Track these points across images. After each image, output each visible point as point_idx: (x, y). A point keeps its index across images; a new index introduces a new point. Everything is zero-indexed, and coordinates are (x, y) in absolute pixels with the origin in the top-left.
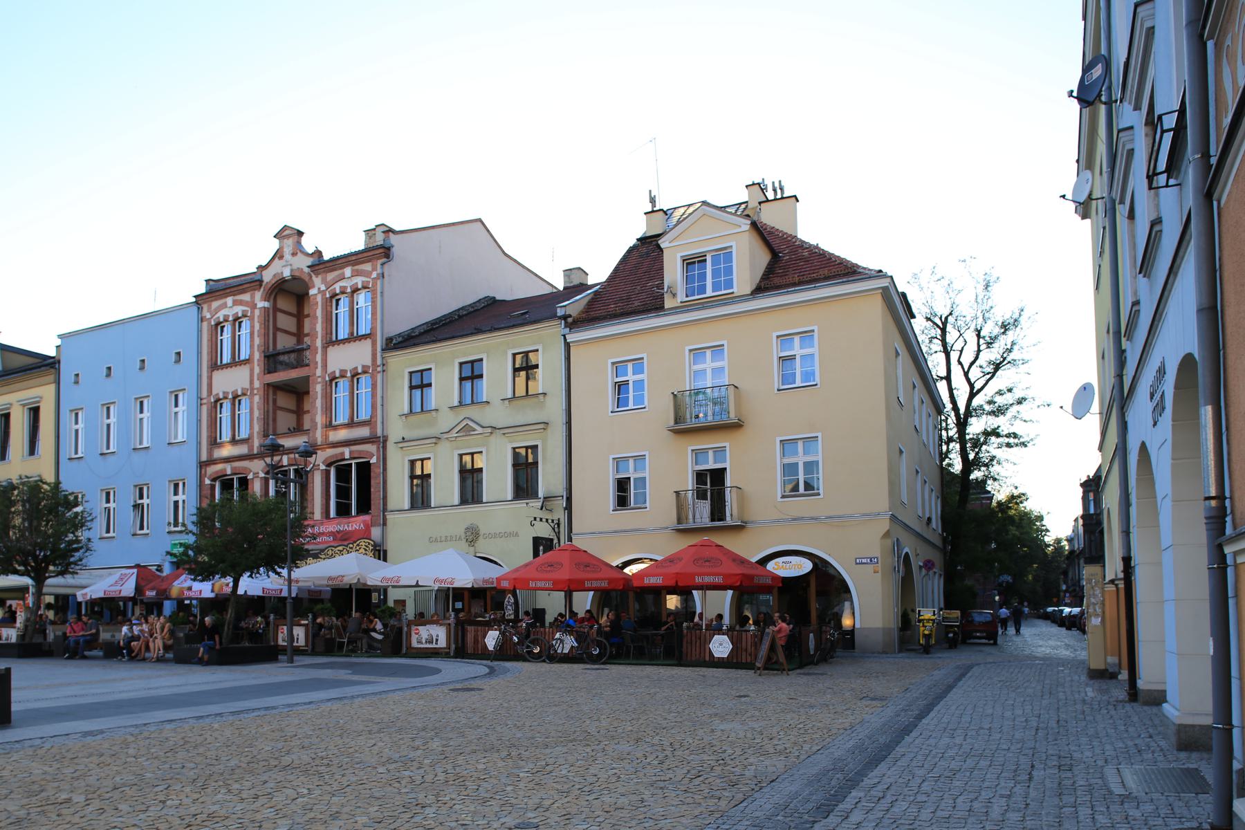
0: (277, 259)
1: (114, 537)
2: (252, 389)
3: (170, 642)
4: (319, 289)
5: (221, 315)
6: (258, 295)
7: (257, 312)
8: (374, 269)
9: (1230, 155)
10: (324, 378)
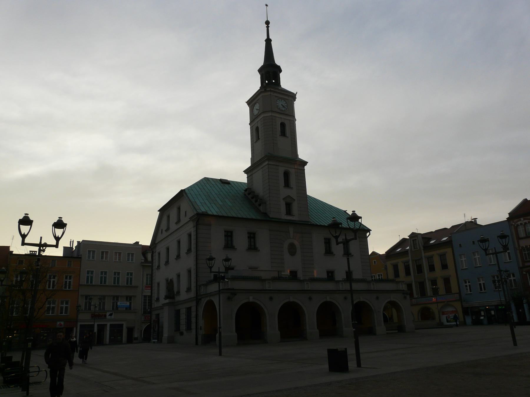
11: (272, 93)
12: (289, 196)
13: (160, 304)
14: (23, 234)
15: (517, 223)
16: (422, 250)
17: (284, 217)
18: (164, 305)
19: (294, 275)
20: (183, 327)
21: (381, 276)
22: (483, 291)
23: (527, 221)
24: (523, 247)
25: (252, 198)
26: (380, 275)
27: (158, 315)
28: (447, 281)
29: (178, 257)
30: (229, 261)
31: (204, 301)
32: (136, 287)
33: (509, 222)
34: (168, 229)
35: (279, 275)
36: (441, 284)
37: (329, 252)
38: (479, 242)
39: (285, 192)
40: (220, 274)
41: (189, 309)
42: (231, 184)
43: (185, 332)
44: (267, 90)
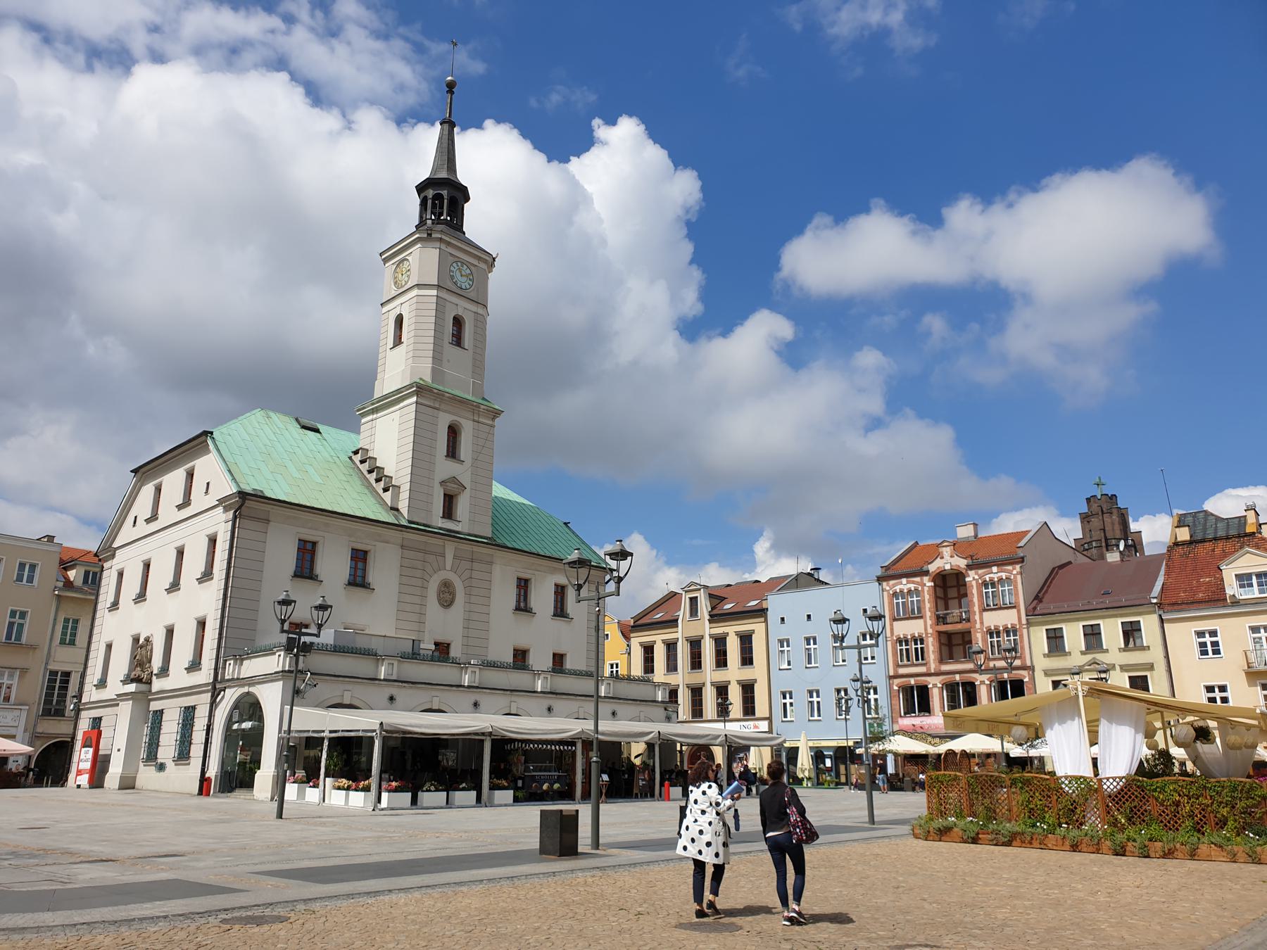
0: (939, 558)
1: (792, 721)
2: (927, 634)
3: (584, 781)
4: (974, 578)
5: (898, 588)
6: (926, 579)
7: (926, 589)
8: (1014, 569)
9: (221, 732)
10: (982, 630)
12: (454, 480)
13: (108, 694)
16: (707, 622)
17: (440, 523)
18: (122, 697)
19: (442, 649)
20: (167, 751)
21: (617, 667)
22: (816, 717)
25: (370, 472)
26: (615, 666)
27: (97, 722)
28: (748, 689)
29: (175, 586)
30: (291, 605)
31: (230, 696)
32: (32, 647)
33: (880, 584)
34: (153, 518)
35: (413, 650)
36: (735, 695)
37: (523, 607)
38: (832, 622)
40: (302, 637)
41: (189, 713)
42: (320, 433)
43: (170, 765)
44: (433, 236)
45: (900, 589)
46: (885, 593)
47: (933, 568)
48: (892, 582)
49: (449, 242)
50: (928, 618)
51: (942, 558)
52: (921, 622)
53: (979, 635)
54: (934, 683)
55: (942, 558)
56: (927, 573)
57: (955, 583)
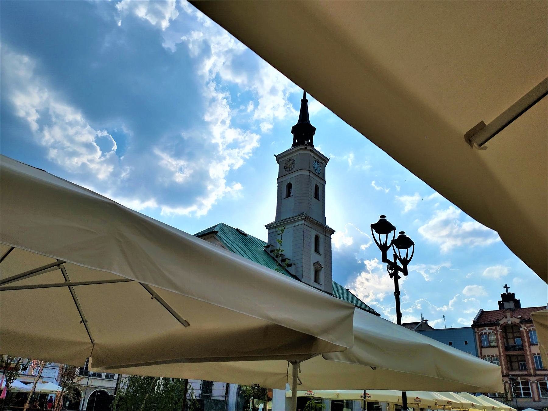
0: (504, 318)
2: (500, 355)
4: (524, 329)
6: (498, 328)
11: (311, 153)
14: (402, 259)
15: (481, 331)
23: (491, 331)
24: (534, 354)
33: (473, 329)
39: (315, 257)
45: (485, 332)
46: (477, 334)
47: (501, 322)
48: (480, 329)
49: (314, 152)
50: (501, 348)
51: (506, 318)
52: (497, 349)
53: (529, 357)
54: (506, 380)
55: (506, 318)
56: (498, 325)
57: (511, 331)
